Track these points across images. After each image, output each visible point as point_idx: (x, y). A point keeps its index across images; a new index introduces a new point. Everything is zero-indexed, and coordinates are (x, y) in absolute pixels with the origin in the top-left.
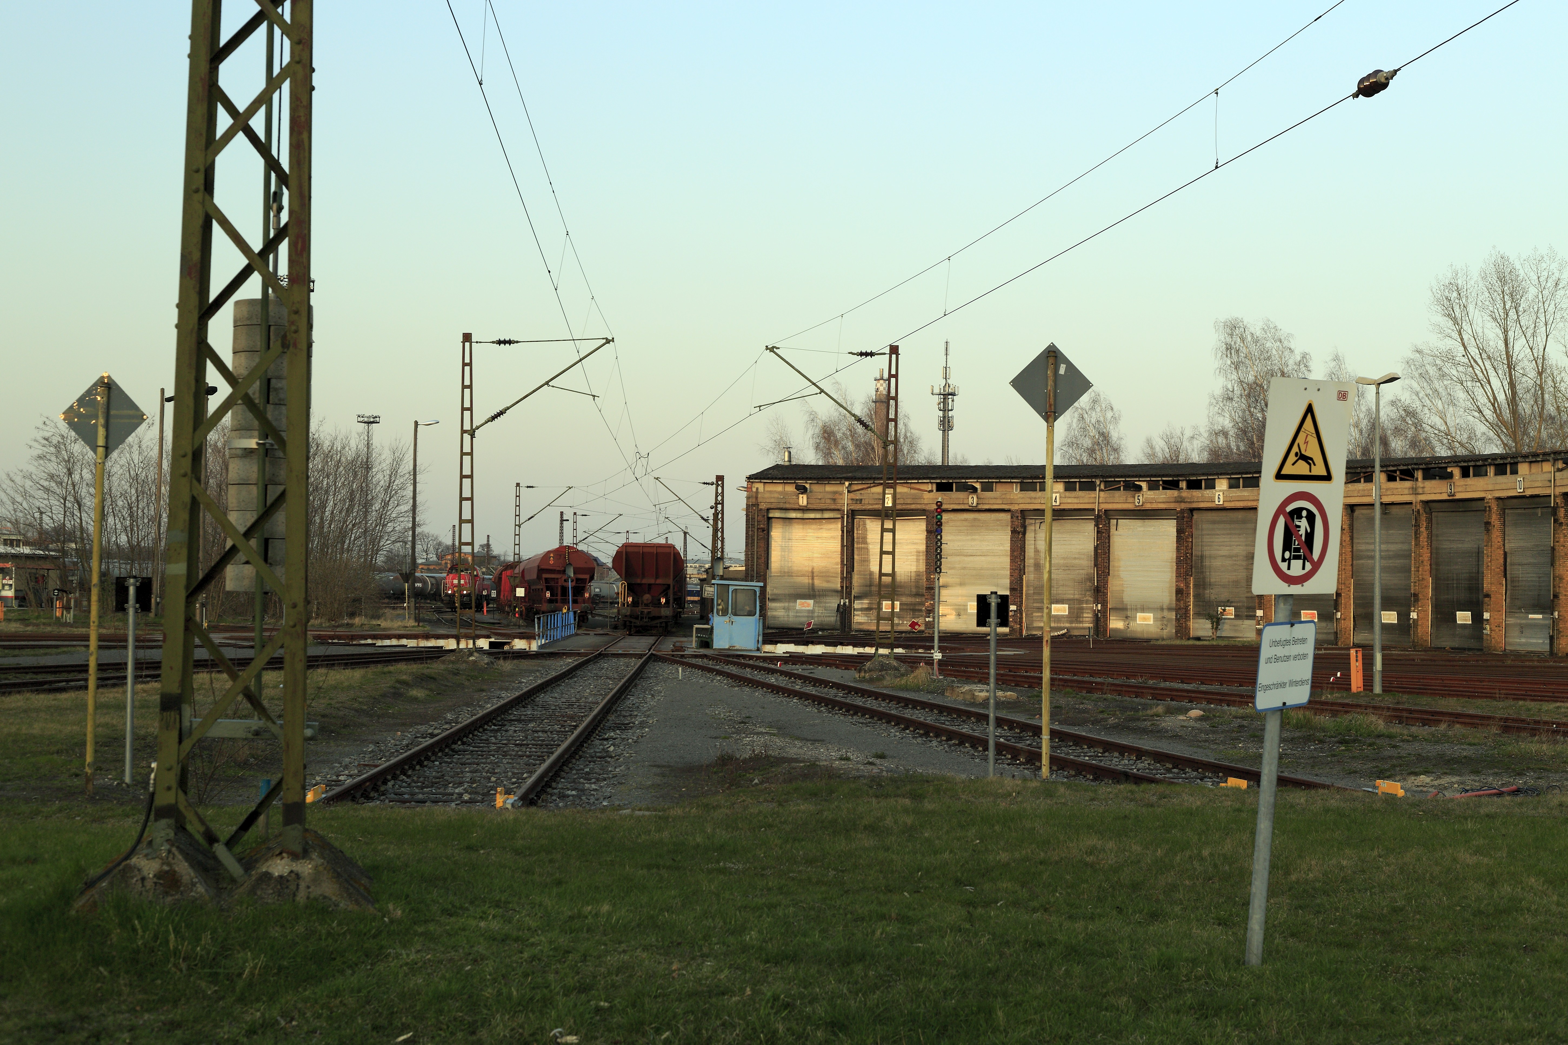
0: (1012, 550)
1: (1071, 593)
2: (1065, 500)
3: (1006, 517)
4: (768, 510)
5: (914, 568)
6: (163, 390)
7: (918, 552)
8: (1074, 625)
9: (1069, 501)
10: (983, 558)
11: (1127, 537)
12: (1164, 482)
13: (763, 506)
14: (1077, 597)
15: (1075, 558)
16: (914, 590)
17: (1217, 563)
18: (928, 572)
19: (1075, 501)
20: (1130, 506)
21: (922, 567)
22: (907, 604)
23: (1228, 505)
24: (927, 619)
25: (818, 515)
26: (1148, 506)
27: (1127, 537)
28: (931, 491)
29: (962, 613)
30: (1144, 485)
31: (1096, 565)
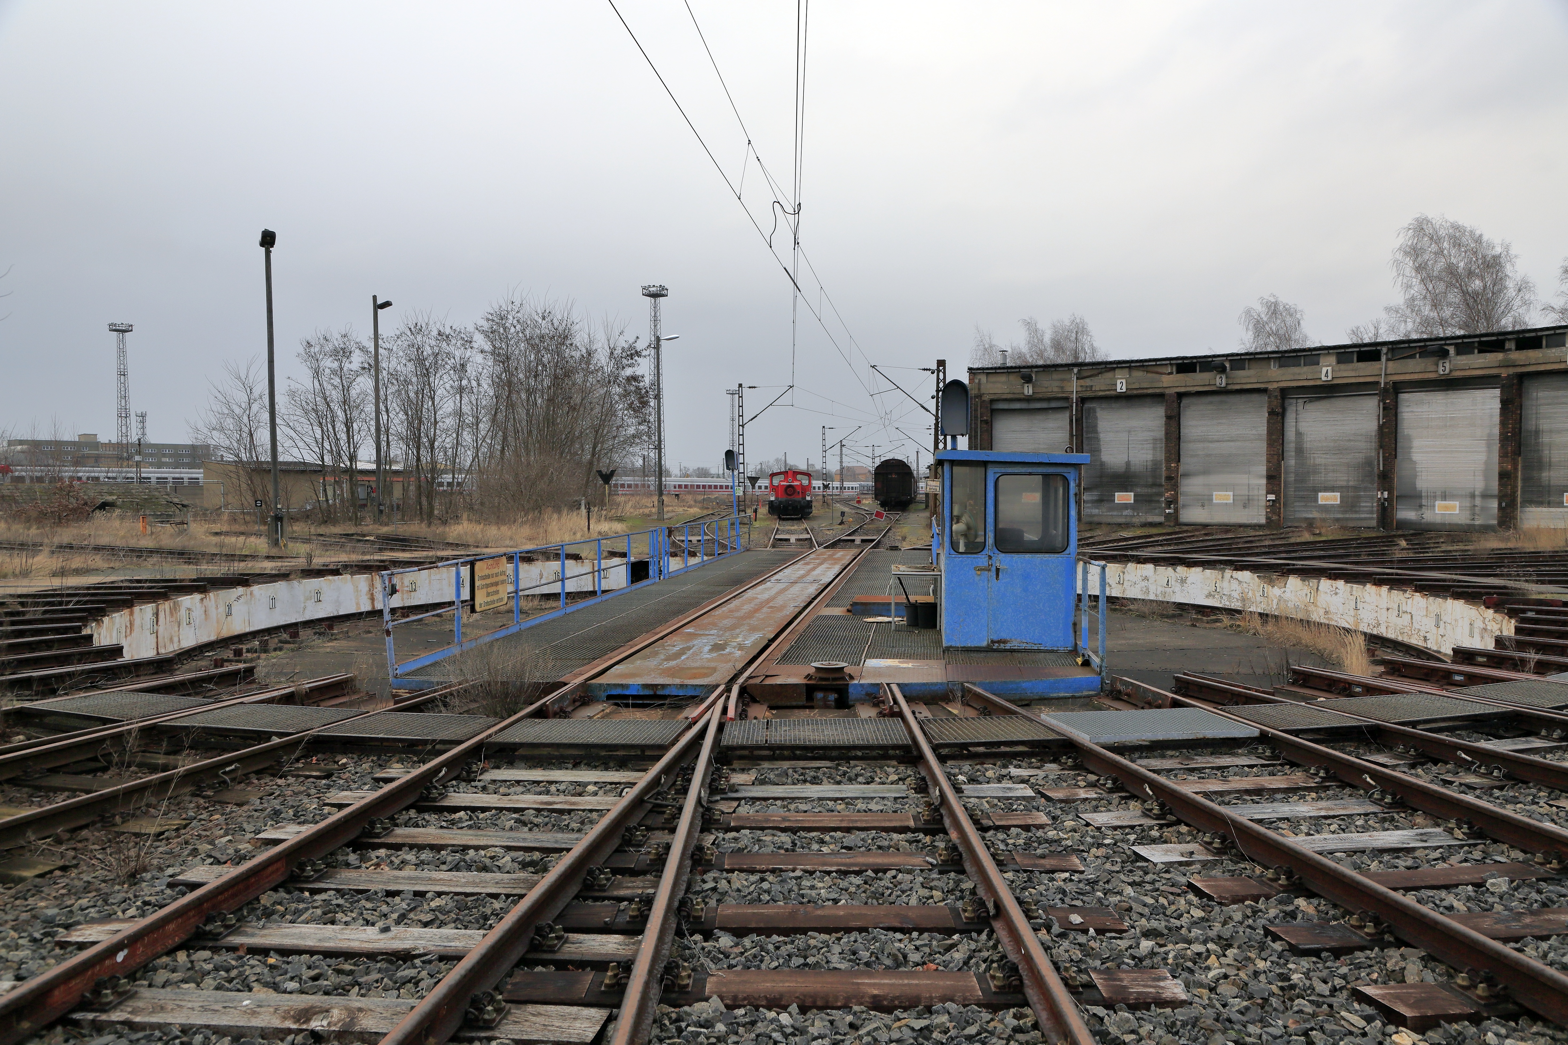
0: (1270, 433)
1: (1342, 478)
3: (1265, 398)
4: (992, 401)
5: (1150, 457)
6: (375, 297)
7: (1155, 440)
8: (1347, 516)
10: (1232, 444)
11: (1421, 412)
12: (1480, 343)
13: (986, 398)
14: (1351, 484)
15: (1350, 440)
16: (1150, 480)
18: (1168, 460)
19: (1353, 374)
20: (1432, 376)
21: (1161, 456)
27: (1421, 412)
28: (1171, 373)
30: (1228, 365)
31: (1381, 446)
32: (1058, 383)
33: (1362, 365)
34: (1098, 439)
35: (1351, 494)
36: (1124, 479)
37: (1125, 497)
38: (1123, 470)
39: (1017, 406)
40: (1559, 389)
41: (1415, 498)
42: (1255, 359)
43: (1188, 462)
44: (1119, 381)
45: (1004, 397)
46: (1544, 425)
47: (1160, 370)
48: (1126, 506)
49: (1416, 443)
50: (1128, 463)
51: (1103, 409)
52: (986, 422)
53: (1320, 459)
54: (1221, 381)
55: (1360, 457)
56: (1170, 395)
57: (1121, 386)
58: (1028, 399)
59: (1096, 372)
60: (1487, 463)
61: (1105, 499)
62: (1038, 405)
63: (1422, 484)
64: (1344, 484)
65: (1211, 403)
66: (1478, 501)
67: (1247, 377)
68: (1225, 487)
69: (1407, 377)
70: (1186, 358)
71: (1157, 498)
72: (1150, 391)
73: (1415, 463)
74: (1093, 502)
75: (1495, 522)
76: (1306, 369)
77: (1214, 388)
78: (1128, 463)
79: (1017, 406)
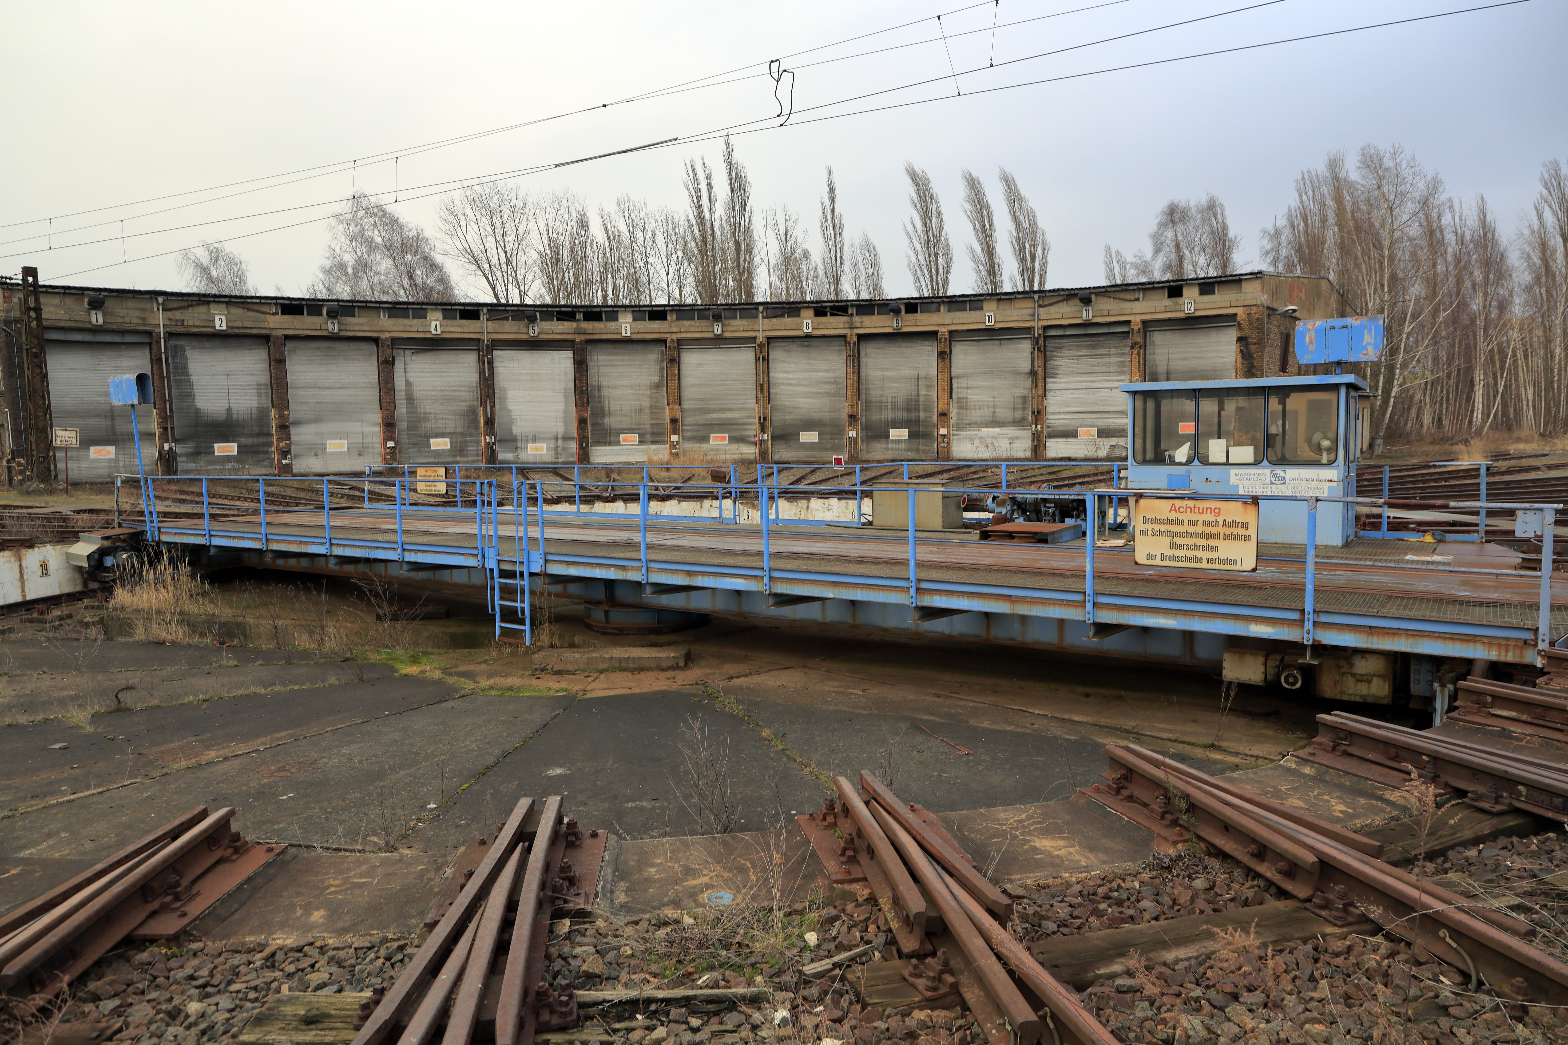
1: (451, 425)
2: (447, 329)
7: (259, 385)
9: (452, 329)
10: (343, 391)
11: (511, 366)
14: (459, 430)
16: (256, 429)
17: (616, 393)
19: (459, 330)
20: (524, 337)
21: (266, 402)
22: (245, 446)
23: (635, 337)
24: (284, 462)
25: (117, 339)
26: (543, 337)
28: (276, 314)
29: (320, 452)
32: (138, 313)
33: (464, 322)
34: (190, 383)
35: (459, 439)
36: (225, 428)
37: (225, 449)
38: (224, 418)
39: (79, 337)
40: (612, 354)
41: (511, 441)
42: (367, 307)
43: (295, 411)
44: (217, 318)
45: (62, 324)
46: (604, 382)
47: (265, 309)
48: (228, 459)
49: (511, 394)
50: (229, 411)
51: (193, 348)
52: (36, 355)
53: (428, 407)
54: (333, 327)
55: (464, 406)
56: (277, 337)
57: (220, 323)
58: (96, 330)
59: (185, 304)
60: (565, 412)
61: (202, 451)
62: (108, 338)
63: (519, 428)
64: (452, 430)
65: (318, 349)
66: (560, 443)
67: (359, 324)
68: (338, 435)
69: (505, 336)
70: (293, 299)
71: (265, 449)
72: (254, 331)
73: (510, 411)
74: (187, 455)
75: (575, 459)
76: (416, 321)
77: (325, 333)
78: (229, 411)
79: (79, 337)
